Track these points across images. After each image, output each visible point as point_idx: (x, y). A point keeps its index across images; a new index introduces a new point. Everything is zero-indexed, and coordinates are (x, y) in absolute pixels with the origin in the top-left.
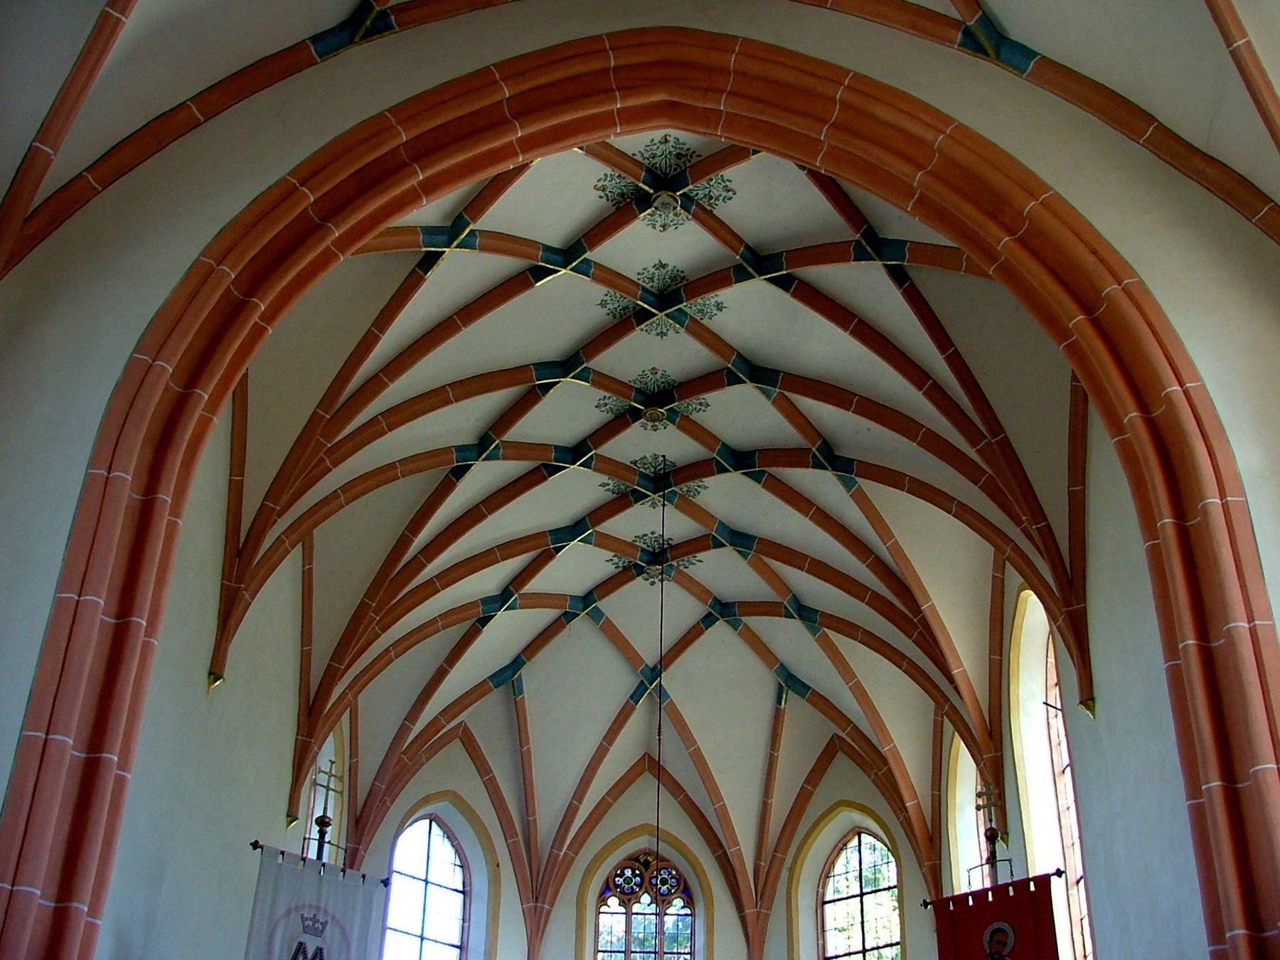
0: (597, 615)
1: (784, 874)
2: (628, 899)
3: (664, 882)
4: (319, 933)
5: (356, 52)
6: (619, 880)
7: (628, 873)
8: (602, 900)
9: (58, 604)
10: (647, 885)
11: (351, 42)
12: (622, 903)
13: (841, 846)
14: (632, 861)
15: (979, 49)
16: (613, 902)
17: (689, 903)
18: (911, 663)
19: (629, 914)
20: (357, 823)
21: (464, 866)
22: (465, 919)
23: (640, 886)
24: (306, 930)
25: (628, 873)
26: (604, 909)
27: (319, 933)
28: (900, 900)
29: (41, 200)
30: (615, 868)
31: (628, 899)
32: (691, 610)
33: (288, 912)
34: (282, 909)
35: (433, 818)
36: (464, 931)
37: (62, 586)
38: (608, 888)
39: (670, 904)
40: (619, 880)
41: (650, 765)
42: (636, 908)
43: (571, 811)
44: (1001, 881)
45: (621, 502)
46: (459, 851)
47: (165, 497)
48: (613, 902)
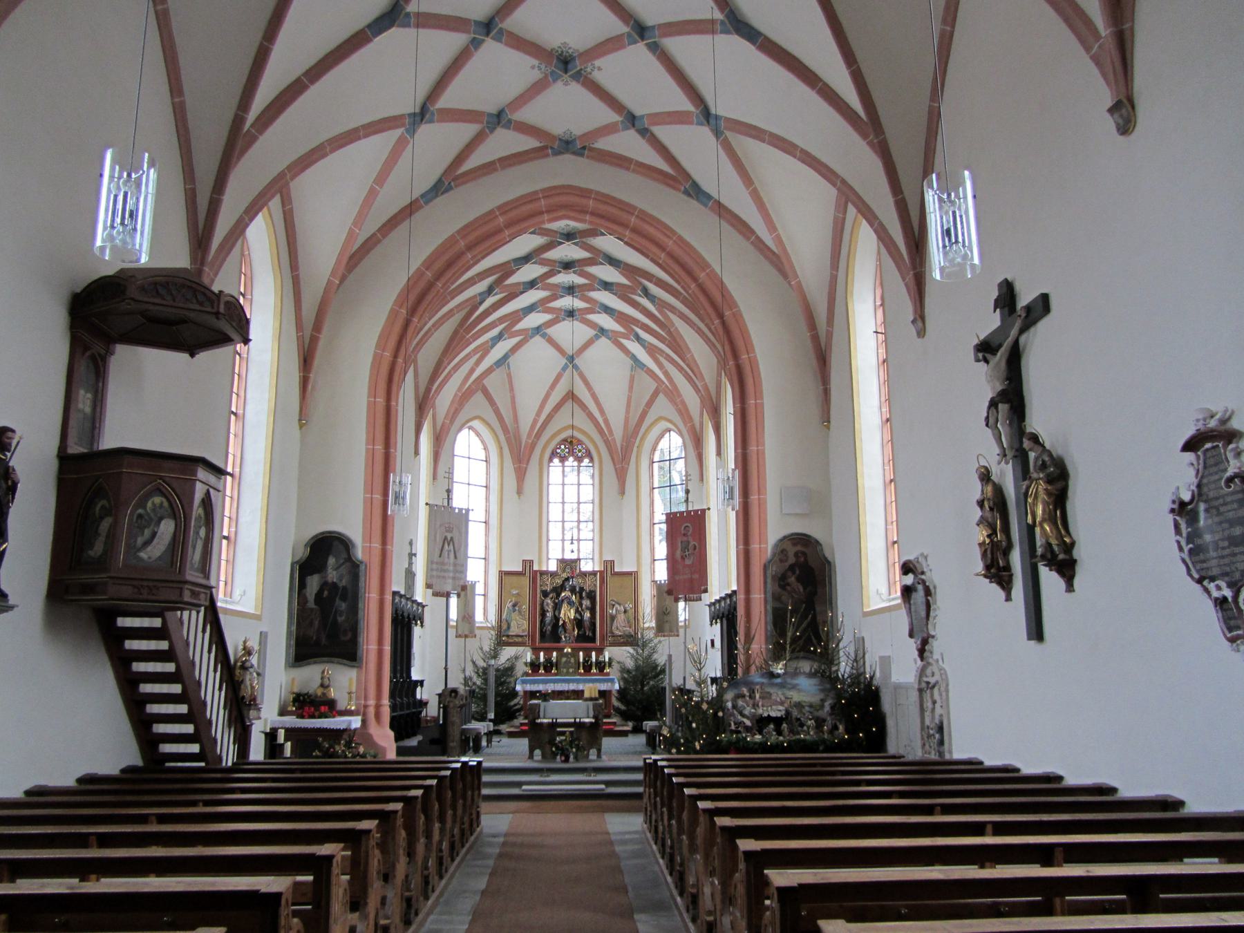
0: (544, 336)
1: (635, 449)
2: (563, 459)
3: (580, 451)
4: (451, 532)
5: (440, 200)
6: (559, 451)
7: (563, 447)
8: (551, 460)
9: (367, 450)
10: (572, 453)
11: (436, 196)
12: (560, 461)
13: (661, 436)
14: (564, 441)
15: (689, 195)
16: (556, 461)
17: (592, 460)
18: (707, 336)
19: (563, 466)
20: (437, 439)
21: (486, 448)
22: (488, 473)
23: (568, 453)
24: (447, 531)
25: (563, 447)
26: (551, 464)
27: (451, 532)
28: (686, 461)
29: (254, 119)
30: (557, 445)
31: (563, 459)
32: (591, 332)
33: (440, 526)
34: (438, 524)
35: (470, 428)
36: (488, 479)
37: (367, 444)
38: (554, 454)
39: (582, 461)
40: (559, 451)
41: (571, 396)
42: (567, 463)
43: (535, 421)
44: (690, 509)
45: (554, 297)
46: (483, 442)
47: (393, 403)
48: (556, 461)
